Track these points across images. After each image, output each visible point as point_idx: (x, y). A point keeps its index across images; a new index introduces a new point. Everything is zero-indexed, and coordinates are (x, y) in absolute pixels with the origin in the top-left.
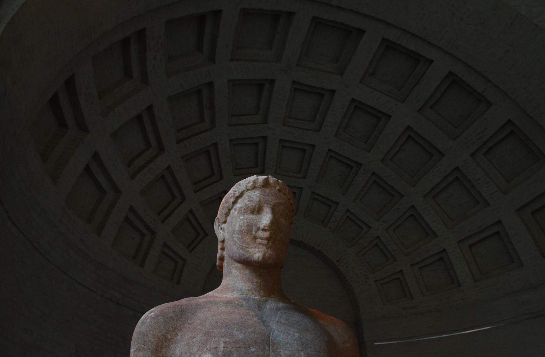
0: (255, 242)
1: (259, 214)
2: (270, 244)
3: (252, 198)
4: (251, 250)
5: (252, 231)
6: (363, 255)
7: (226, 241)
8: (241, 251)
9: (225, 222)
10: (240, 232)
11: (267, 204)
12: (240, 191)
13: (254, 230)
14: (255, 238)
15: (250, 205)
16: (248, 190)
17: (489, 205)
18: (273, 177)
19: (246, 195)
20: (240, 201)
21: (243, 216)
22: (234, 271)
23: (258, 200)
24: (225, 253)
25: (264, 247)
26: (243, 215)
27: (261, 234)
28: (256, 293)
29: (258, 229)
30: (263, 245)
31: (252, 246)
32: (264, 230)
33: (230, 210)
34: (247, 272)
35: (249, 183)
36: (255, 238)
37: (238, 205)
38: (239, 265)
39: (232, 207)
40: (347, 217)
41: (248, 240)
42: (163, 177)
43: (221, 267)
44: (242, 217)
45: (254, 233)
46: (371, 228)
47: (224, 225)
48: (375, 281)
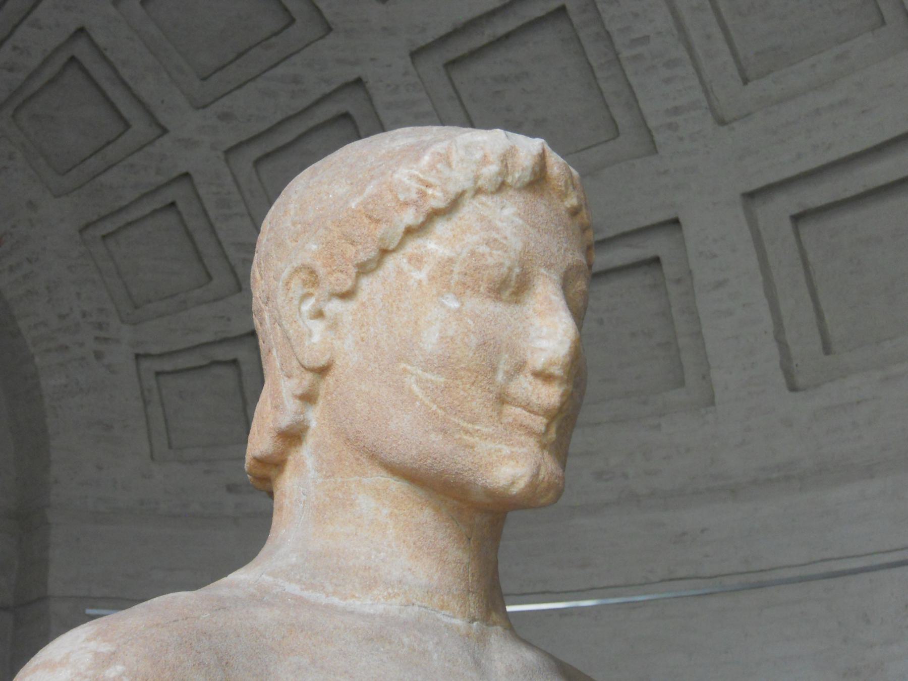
0: (500, 413)
1: (517, 302)
2: (553, 435)
3: (497, 230)
4: (484, 447)
5: (494, 370)
6: (104, 237)
7: (335, 371)
8: (435, 438)
9: (346, 295)
10: (444, 364)
11: (549, 266)
12: (453, 190)
13: (503, 367)
14: (503, 399)
15: (490, 261)
16: (478, 191)
17: (654, 149)
18: (532, 134)
20: (441, 227)
22: (365, 503)
23: (519, 246)
24: (314, 417)
25: (532, 441)
26: (459, 296)
27: (526, 387)
28: (453, 604)
29: (519, 368)
30: (530, 432)
31: (490, 430)
32: (544, 376)
34: (426, 515)
35: (485, 161)
36: (503, 399)
37: (436, 245)
38: (396, 485)
39: (401, 245)
40: (73, 59)
41: (478, 401)
43: (273, 465)
45: (500, 377)
46: (165, 131)
47: (334, 307)
48: (138, 356)
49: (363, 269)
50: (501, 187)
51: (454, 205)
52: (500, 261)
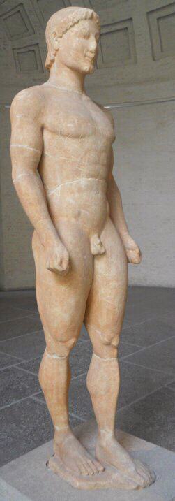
8: (74, 62)
9: (61, 37)
13: (85, 50)
14: (85, 56)
19: (80, 23)
20: (76, 26)
21: (70, 35)
22: (64, 73)
24: (56, 58)
27: (88, 54)
29: (88, 50)
32: (91, 52)
33: (67, 30)
36: (85, 56)
37: (75, 29)
38: (69, 70)
42: (101, 35)
43: (50, 66)
44: (78, 39)
47: (59, 39)
49: (64, 33)
50: (86, 19)
51: (78, 22)
52: (85, 32)
